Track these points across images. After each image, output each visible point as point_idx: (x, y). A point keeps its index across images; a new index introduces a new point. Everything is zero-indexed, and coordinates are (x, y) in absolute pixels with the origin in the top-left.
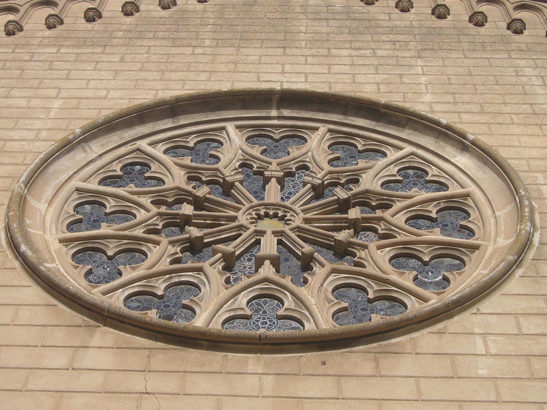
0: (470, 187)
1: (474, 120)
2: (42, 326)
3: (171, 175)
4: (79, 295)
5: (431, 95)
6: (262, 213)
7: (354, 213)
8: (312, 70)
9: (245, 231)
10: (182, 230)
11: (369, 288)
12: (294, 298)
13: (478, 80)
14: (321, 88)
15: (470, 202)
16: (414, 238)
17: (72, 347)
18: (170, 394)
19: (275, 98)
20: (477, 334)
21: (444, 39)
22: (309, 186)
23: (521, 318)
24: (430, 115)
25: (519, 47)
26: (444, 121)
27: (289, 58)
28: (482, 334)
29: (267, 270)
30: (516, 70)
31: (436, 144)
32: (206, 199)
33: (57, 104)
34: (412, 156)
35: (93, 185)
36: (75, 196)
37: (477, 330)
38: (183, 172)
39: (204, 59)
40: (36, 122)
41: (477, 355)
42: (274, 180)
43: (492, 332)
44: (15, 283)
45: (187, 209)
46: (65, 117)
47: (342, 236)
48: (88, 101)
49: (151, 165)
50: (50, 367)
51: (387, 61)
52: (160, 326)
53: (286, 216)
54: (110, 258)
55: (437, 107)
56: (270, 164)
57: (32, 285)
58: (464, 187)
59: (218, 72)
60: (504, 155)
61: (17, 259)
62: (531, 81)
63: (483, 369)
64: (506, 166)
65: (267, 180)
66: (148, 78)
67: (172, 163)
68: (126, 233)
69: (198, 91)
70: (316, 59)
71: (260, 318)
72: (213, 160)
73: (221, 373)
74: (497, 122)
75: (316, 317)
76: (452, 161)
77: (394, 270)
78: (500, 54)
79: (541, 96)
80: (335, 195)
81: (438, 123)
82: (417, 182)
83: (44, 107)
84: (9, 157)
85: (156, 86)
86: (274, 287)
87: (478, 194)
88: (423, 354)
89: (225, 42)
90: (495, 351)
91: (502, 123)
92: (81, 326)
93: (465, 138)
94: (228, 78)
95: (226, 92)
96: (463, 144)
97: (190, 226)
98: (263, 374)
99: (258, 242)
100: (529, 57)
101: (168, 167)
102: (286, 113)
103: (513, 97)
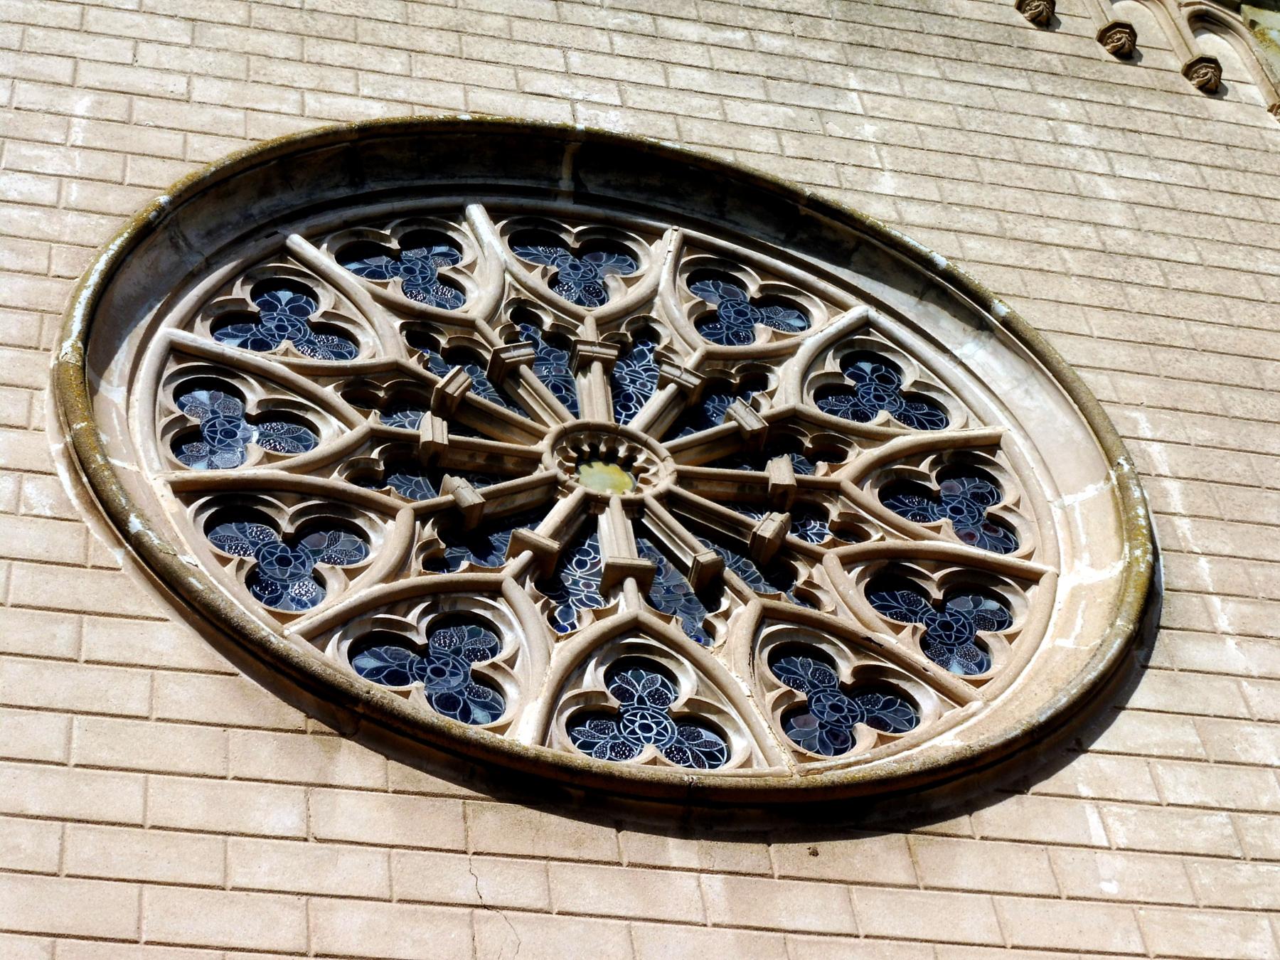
0: (1000, 424)
1: (992, 255)
2: (221, 725)
4: (296, 660)
5: (892, 177)
7: (780, 471)
8: (630, 73)
9: (565, 495)
10: (437, 486)
11: (840, 657)
12: (701, 674)
13: (981, 146)
15: (1000, 458)
16: (911, 544)
17: (300, 784)
18: (531, 911)
20: (1084, 798)
21: (891, 21)
22: (671, 387)
23: (1160, 768)
24: (896, 232)
25: (1048, 63)
27: (573, 33)
28: (1093, 799)
30: (1051, 128)
31: (920, 307)
32: (464, 402)
33: (81, 104)
37: (1084, 791)
38: (398, 322)
39: (385, 12)
40: (45, 152)
41: (1093, 847)
43: (1112, 796)
44: (131, 609)
45: (432, 429)
46: (109, 148)
47: (768, 525)
48: (154, 106)
49: (318, 290)
50: (267, 833)
51: (785, 69)
55: (913, 213)
57: (168, 617)
58: (987, 420)
59: (424, 52)
60: (1069, 357)
61: (120, 544)
62: (1087, 162)
63: (1110, 881)
64: (1083, 395)
66: (271, 53)
67: (369, 295)
70: (632, 42)
71: (635, 715)
72: (450, 293)
73: (619, 864)
74: (1037, 266)
75: (757, 729)
76: (957, 353)
77: (882, 620)
78: (1014, 79)
79: (1112, 205)
80: (730, 418)
81: (928, 262)
82: (882, 393)
83: (53, 110)
84: (12, 250)
85: (296, 78)
86: (300, 400)
88: (995, 839)
89: (1223, 457)
90: (1125, 841)
91: (1048, 271)
92: (304, 732)
93: (988, 308)
94: (451, 75)
97: (452, 475)
98: (702, 871)
100: (1071, 96)
103: (1057, 200)
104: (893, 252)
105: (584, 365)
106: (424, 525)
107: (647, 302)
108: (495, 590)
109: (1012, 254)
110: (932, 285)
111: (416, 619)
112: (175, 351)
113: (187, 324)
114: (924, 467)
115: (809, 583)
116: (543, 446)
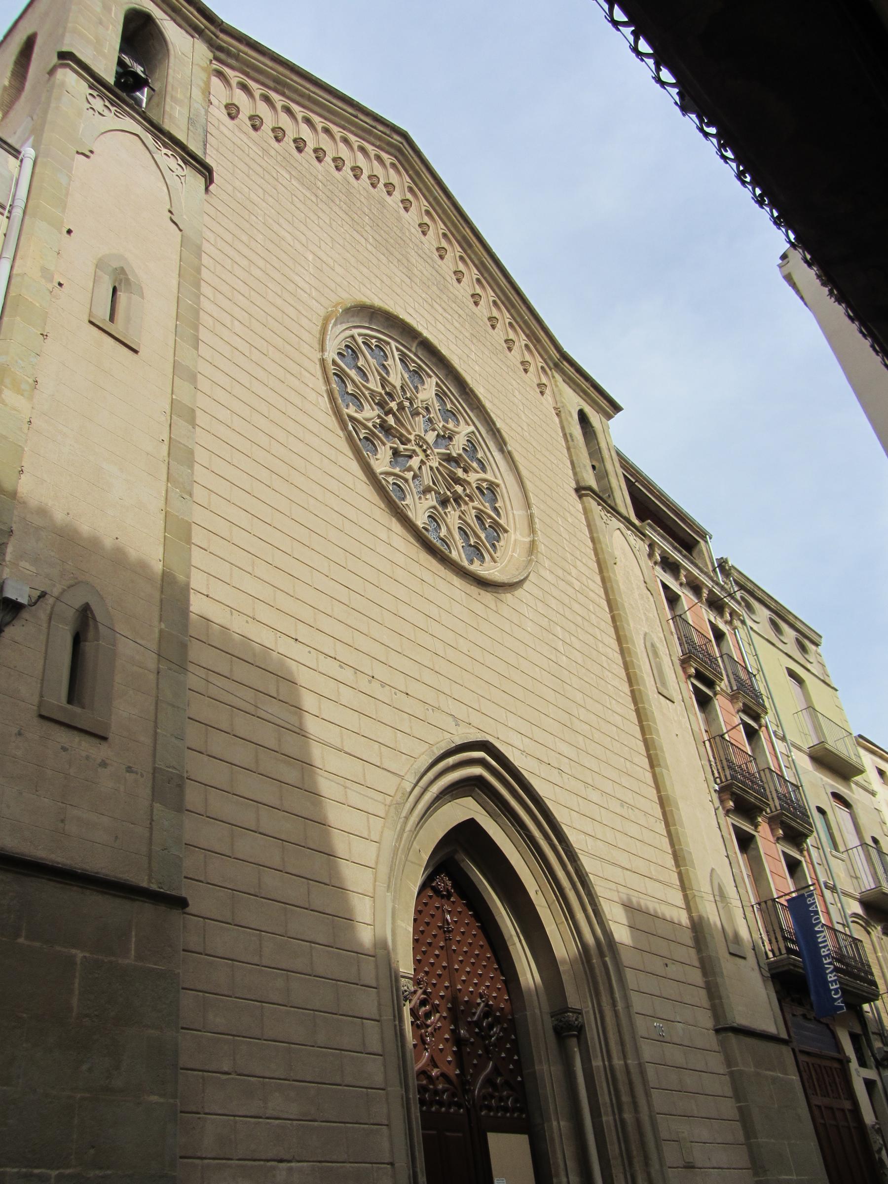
3: (848, 870)
14: (444, 351)
15: (498, 490)
26: (499, 425)
29: (409, 475)
42: (436, 432)
44: (346, 453)
53: (373, 393)
56: (440, 422)
69: (141, 8)
80: (448, 450)
81: (494, 424)
87: (502, 486)
96: (502, 447)
99: (410, 457)
104: (485, 414)
105: (434, 430)
106: (378, 419)
107: (458, 433)
108: (384, 444)
109: (598, 633)
110: (492, 430)
111: (363, 433)
112: (352, 337)
113: (360, 335)
114: (489, 521)
115: (449, 512)
116: (414, 433)
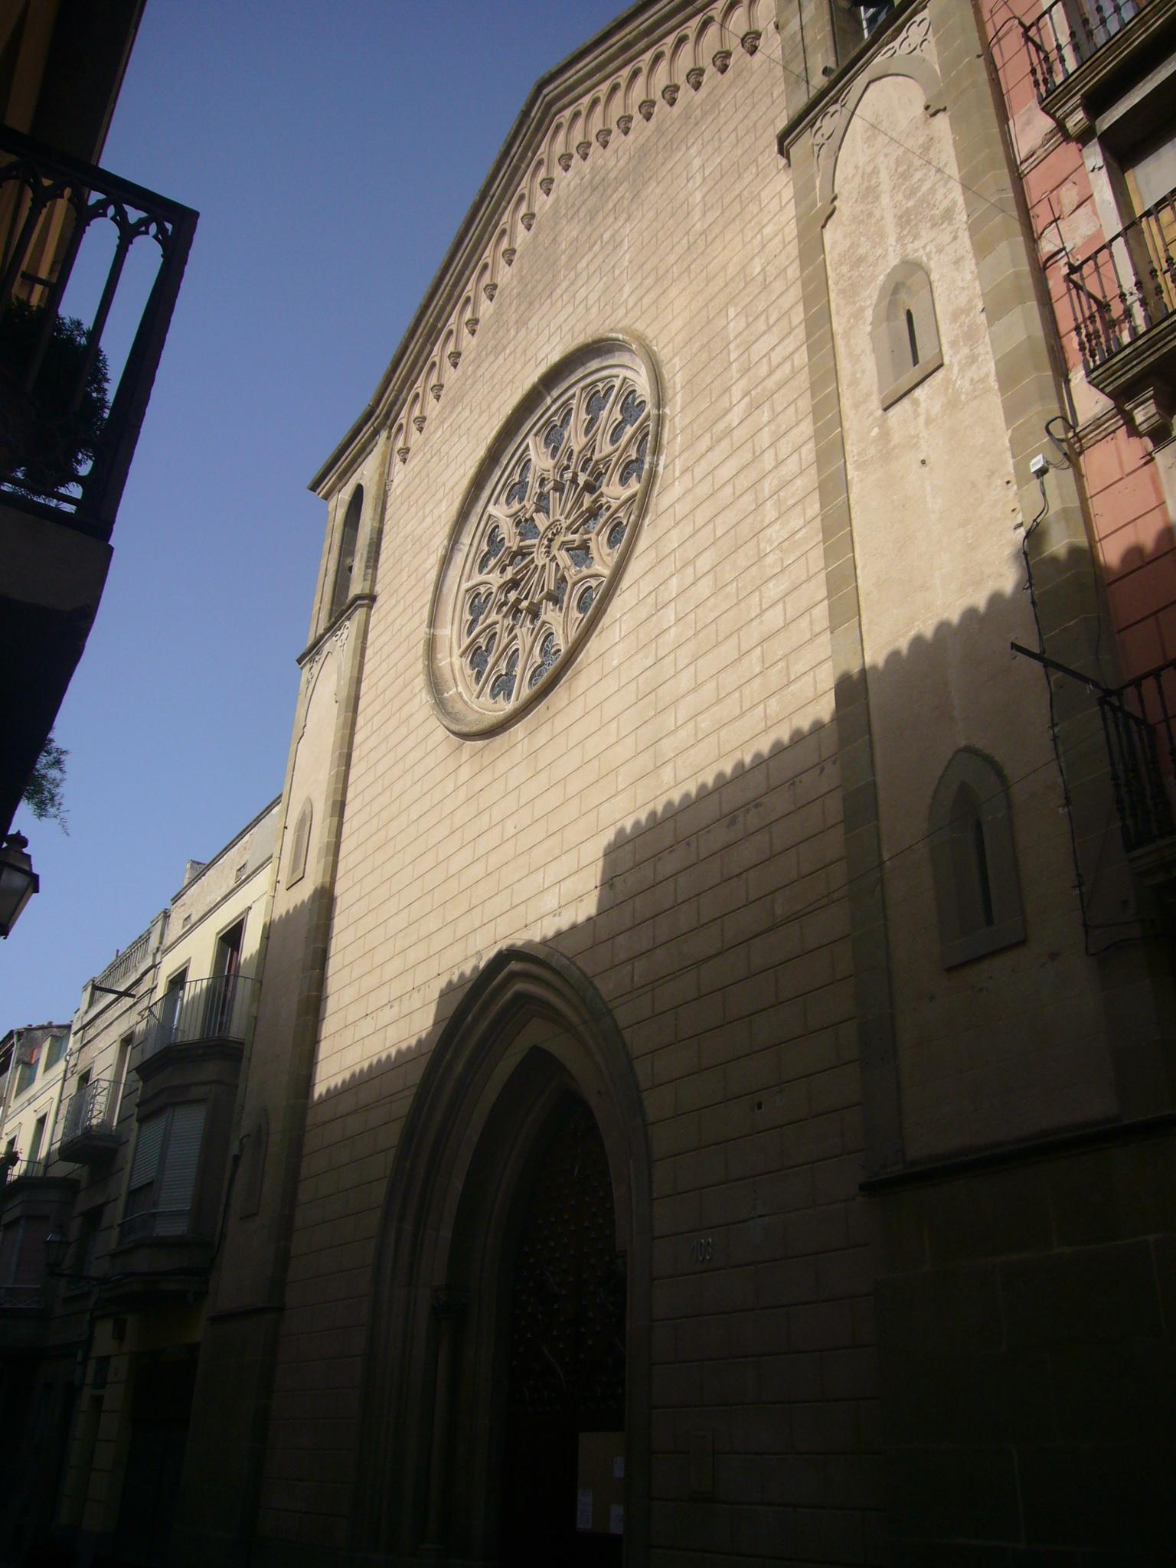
6: (546, 543)
19: (540, 387)
34: (359, 602)
35: (466, 641)
36: (464, 659)
52: (536, 693)
54: (506, 674)
65: (532, 519)
68: (500, 649)
95: (512, 413)
101: (353, 701)
102: (555, 393)
